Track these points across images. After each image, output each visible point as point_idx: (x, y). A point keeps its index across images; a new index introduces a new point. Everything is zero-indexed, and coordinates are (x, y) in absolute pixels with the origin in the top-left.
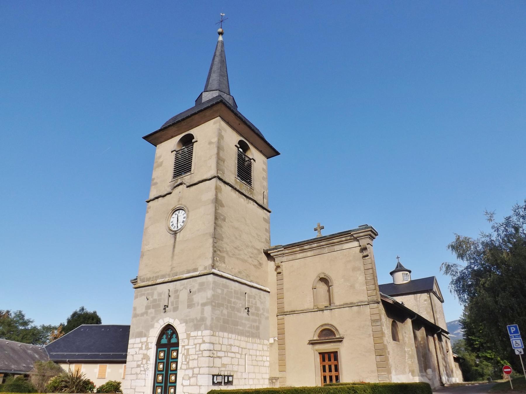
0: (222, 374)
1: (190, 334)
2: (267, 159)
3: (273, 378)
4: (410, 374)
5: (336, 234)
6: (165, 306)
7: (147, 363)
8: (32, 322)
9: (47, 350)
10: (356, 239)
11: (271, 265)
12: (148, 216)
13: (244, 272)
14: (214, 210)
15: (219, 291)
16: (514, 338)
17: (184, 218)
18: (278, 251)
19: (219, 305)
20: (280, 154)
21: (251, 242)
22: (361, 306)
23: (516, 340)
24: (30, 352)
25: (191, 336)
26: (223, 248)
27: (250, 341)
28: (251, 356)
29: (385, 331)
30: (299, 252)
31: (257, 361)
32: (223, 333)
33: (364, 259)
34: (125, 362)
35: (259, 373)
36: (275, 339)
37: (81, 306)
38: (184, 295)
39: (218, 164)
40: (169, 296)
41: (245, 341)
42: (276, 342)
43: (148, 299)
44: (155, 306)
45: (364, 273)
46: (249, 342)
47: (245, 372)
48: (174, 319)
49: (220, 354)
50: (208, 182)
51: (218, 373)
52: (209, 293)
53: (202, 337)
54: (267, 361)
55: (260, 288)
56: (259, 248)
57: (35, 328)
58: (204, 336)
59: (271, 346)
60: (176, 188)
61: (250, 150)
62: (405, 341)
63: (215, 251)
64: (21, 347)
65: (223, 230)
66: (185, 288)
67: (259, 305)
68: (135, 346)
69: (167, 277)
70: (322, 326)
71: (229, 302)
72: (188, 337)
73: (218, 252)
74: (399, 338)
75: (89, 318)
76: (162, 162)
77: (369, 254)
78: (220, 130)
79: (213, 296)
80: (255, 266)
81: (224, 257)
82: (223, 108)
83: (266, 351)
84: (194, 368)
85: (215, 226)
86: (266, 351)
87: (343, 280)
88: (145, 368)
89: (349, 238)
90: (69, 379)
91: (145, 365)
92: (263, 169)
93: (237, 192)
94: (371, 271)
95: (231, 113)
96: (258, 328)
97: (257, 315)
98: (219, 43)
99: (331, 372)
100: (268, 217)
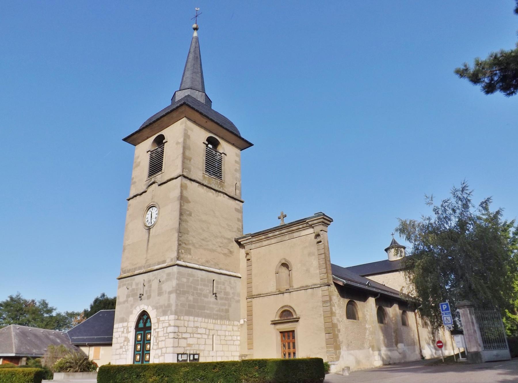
0: (187, 353)
1: (159, 318)
2: (241, 151)
3: (243, 355)
4: (371, 349)
5: (294, 222)
6: (140, 294)
7: (127, 345)
8: (55, 309)
9: (69, 335)
10: (311, 226)
11: (243, 252)
12: (129, 213)
13: (212, 261)
14: (179, 206)
15: (185, 280)
16: (446, 314)
17: (157, 214)
18: (247, 240)
19: (184, 293)
20: (253, 145)
21: (220, 232)
22: (315, 288)
23: (446, 317)
24: (52, 338)
25: (160, 320)
26: (189, 241)
27: (219, 323)
28: (219, 336)
29: (335, 310)
30: (265, 240)
31: (226, 341)
32: (188, 317)
33: (318, 244)
34: (110, 345)
35: (228, 351)
36: (244, 320)
37: (102, 293)
38: (155, 284)
39: (184, 163)
40: (144, 286)
41: (213, 323)
42: (245, 322)
43: (128, 289)
44: (134, 295)
45: (317, 258)
46: (217, 324)
47: (213, 350)
48: (147, 305)
49: (185, 336)
50: (174, 180)
51: (183, 352)
52: (174, 283)
53: (168, 321)
54: (237, 340)
55: (230, 274)
56: (229, 237)
57: (59, 315)
58: (170, 320)
59: (241, 327)
60: (150, 186)
61: (221, 146)
62: (367, 319)
63: (179, 245)
64: (44, 333)
65: (189, 224)
66: (156, 278)
67: (228, 289)
68: (119, 330)
69: (143, 268)
70: (282, 307)
71: (196, 289)
72: (158, 321)
73: (184, 245)
74: (359, 316)
75: (109, 304)
76: (140, 162)
77: (322, 240)
78: (185, 130)
79: (178, 284)
80: (225, 254)
81: (190, 249)
82: (187, 109)
83: (237, 331)
84: (162, 348)
85: (179, 221)
86: (237, 331)
87: (300, 265)
88: (126, 349)
89: (305, 225)
90: (73, 360)
91: (126, 347)
92: (236, 162)
93: (205, 188)
94: (323, 256)
95: (195, 112)
96: (227, 311)
97: (226, 299)
98: (193, 39)
99: (290, 349)
100: (240, 207)
